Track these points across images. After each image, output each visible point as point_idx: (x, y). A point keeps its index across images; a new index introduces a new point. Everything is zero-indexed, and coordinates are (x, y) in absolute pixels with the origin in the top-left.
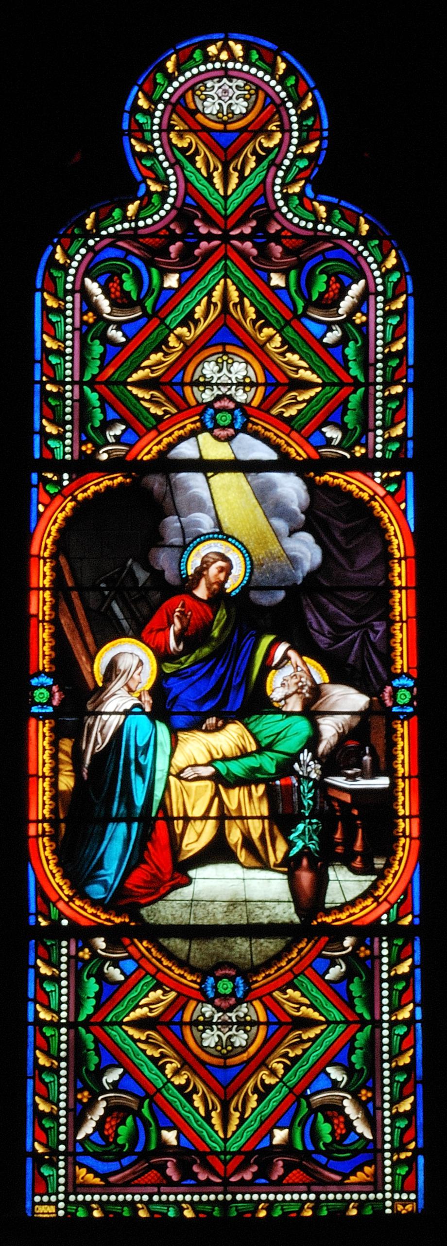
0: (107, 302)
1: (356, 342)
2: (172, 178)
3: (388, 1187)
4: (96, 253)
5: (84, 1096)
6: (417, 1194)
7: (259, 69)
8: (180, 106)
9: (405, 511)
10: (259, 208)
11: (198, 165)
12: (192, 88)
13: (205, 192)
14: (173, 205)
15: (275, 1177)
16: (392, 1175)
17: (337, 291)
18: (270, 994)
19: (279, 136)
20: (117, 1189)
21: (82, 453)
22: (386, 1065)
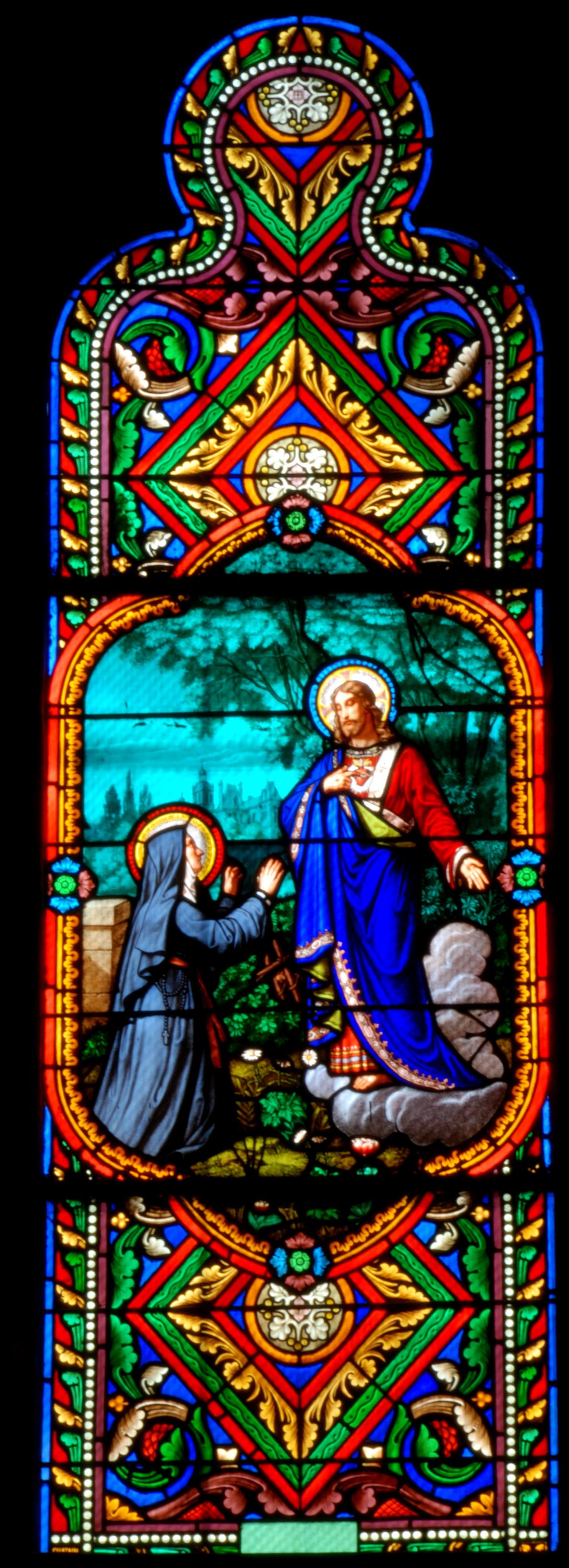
0: (461, 1421)
1: (122, 1373)
2: (228, 208)
3: (512, 1521)
4: (131, 309)
5: (118, 1403)
6: (548, 1529)
7: (345, 64)
8: (236, 114)
9: (532, 642)
10: (345, 244)
11: (263, 191)
12: (254, 91)
13: (272, 227)
14: (230, 245)
15: (364, 1511)
16: (517, 1505)
17: (147, 1444)
18: (359, 1270)
19: (367, 149)
20: (161, 1528)
21: (488, 1206)
22: (510, 1357)
